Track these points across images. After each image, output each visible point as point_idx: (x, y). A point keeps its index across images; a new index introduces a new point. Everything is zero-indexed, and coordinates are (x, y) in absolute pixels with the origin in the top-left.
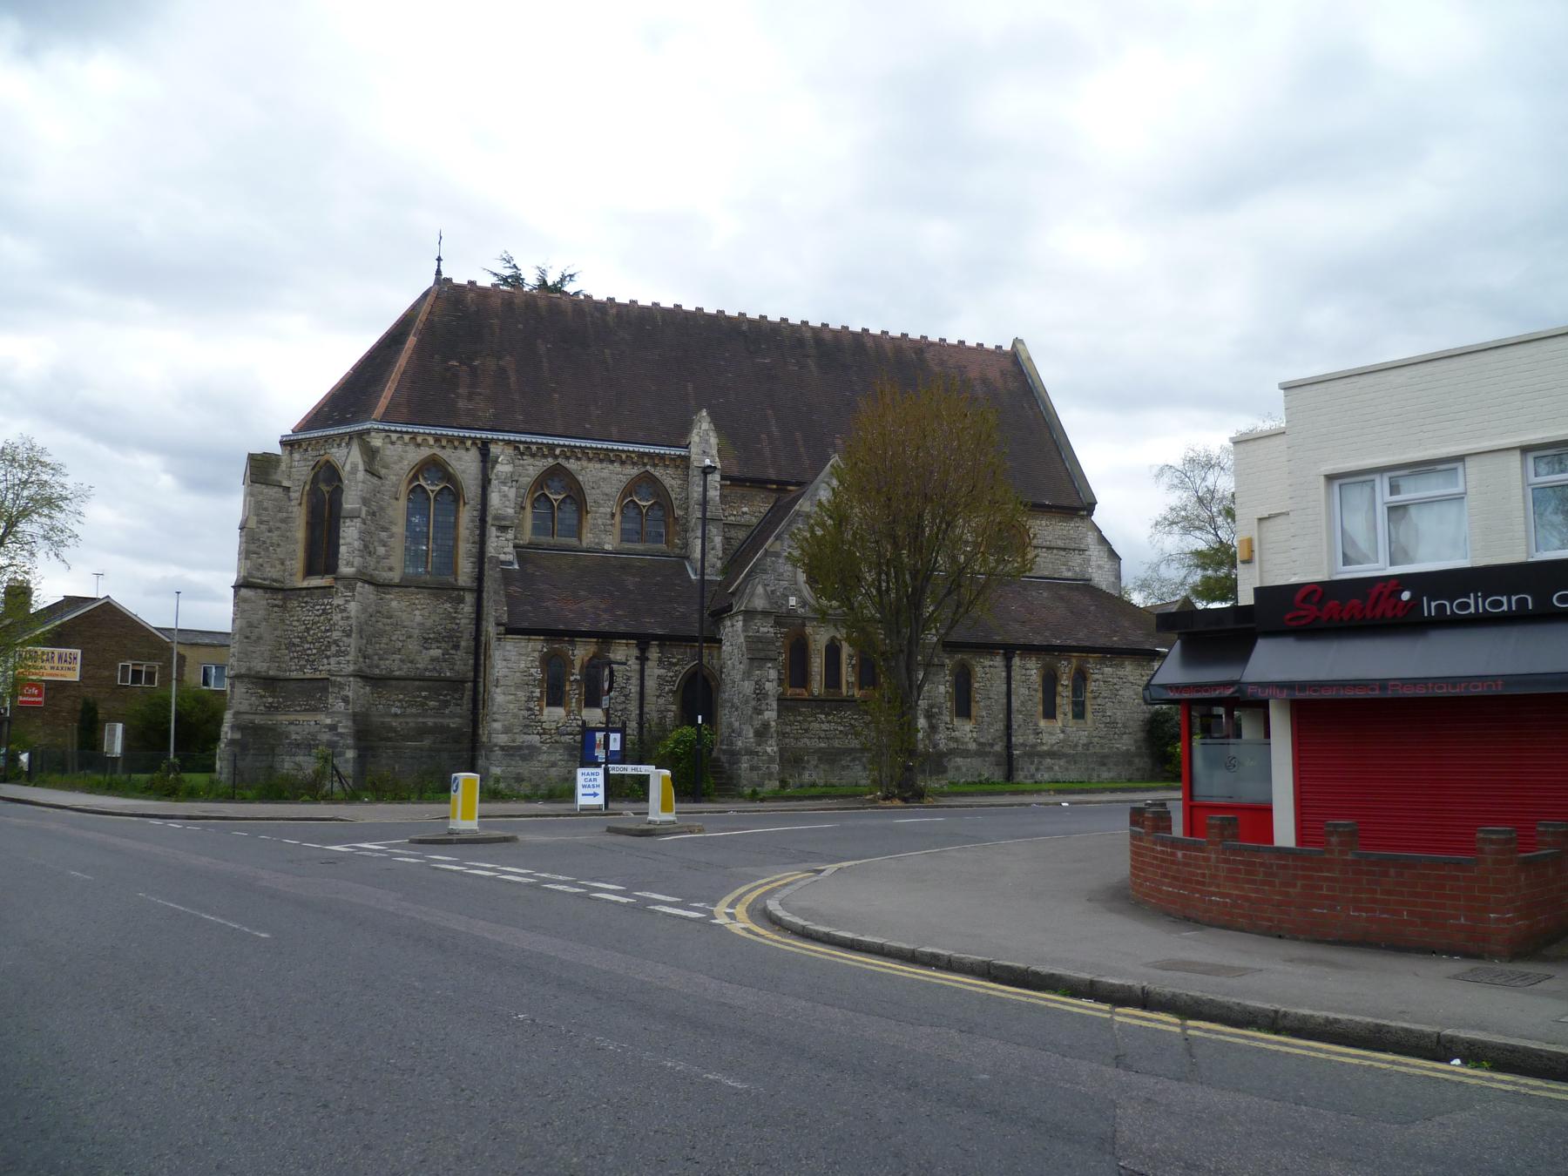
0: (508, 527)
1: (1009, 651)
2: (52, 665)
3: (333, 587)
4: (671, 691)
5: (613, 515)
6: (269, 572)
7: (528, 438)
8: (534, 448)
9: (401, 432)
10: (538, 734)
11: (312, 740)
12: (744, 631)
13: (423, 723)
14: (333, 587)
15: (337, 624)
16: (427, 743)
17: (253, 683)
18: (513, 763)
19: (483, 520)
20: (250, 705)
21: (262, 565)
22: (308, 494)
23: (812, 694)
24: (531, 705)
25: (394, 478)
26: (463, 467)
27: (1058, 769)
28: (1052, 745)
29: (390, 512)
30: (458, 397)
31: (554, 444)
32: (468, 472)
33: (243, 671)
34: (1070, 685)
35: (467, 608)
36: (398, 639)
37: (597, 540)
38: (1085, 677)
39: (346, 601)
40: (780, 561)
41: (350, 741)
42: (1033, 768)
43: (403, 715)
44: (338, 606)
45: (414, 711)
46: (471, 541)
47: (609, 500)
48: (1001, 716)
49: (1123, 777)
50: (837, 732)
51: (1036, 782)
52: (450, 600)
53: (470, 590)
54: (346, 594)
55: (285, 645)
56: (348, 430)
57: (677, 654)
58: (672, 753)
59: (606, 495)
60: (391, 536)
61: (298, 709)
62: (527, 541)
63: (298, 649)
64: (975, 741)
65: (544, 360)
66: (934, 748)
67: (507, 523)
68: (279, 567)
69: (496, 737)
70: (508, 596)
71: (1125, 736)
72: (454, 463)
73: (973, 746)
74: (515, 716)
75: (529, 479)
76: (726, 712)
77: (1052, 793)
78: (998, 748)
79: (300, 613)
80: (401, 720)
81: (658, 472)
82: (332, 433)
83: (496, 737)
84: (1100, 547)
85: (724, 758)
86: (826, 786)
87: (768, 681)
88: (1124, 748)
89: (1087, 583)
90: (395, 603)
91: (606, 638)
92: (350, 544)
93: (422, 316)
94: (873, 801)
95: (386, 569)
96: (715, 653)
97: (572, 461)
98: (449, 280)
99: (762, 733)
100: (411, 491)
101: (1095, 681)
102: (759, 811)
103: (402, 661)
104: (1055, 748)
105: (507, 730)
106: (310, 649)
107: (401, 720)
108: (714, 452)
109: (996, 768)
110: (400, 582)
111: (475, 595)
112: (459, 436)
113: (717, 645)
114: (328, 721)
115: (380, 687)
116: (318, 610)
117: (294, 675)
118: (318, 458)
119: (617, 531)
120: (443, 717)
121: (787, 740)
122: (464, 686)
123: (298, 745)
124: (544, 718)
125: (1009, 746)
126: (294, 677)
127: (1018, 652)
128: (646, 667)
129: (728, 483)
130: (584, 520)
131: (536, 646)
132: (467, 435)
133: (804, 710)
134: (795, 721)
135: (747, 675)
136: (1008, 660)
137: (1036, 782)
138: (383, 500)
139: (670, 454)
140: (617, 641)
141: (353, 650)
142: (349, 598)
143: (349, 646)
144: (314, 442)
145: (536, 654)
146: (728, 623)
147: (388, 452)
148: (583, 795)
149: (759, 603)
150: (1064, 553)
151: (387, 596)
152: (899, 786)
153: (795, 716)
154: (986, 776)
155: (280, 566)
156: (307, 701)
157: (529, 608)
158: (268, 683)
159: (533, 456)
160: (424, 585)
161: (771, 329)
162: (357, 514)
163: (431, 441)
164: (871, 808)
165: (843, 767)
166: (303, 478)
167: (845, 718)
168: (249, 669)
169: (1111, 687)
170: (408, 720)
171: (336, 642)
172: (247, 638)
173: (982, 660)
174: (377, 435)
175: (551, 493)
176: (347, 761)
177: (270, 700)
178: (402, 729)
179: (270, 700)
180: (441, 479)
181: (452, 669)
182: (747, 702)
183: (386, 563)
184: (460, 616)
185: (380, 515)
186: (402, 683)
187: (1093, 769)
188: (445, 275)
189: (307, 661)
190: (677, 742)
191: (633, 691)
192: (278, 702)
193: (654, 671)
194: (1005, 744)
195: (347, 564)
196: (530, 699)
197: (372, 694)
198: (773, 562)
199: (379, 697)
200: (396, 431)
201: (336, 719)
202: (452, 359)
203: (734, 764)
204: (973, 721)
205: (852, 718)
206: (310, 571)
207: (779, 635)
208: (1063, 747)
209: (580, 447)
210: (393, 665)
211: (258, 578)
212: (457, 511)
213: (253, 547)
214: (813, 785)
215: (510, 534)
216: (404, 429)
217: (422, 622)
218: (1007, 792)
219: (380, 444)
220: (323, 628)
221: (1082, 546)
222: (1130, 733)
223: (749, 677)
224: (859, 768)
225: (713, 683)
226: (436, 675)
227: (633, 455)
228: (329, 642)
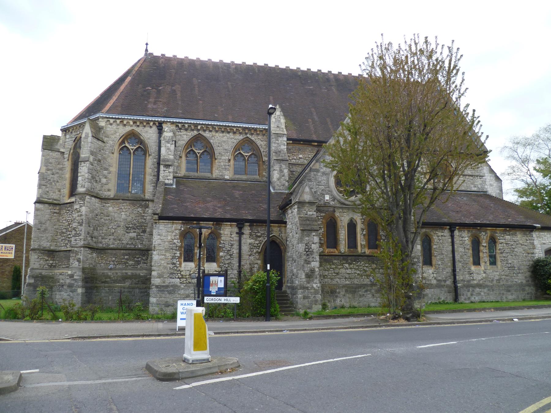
0: (170, 165)
1: (452, 227)
2: (2, 251)
4: (257, 252)
5: (229, 160)
6: (52, 195)
7: (183, 121)
8: (186, 125)
9: (115, 118)
10: (178, 278)
12: (298, 214)
13: (126, 273)
16: (127, 284)
17: (42, 253)
18: (164, 295)
19: (159, 164)
21: (48, 192)
22: (72, 155)
23: (341, 252)
24: (175, 261)
25: (112, 142)
27: (483, 294)
28: (479, 280)
29: (109, 160)
30: (148, 103)
31: (197, 123)
32: (151, 138)
34: (487, 246)
36: (112, 228)
38: (495, 241)
39: (80, 206)
40: (319, 174)
41: (80, 283)
42: (469, 294)
43: (114, 269)
44: (77, 209)
45: (121, 266)
46: (152, 175)
47: (227, 152)
48: (450, 264)
49: (520, 298)
50: (356, 275)
51: (472, 302)
52: (141, 206)
54: (80, 202)
55: (60, 233)
57: (261, 230)
58: (252, 289)
59: (226, 150)
60: (110, 173)
61: (64, 266)
62: (183, 175)
63: (65, 235)
64: (435, 279)
65: (196, 87)
66: (416, 283)
67: (169, 163)
70: (165, 200)
71: (519, 275)
72: (143, 134)
73: (434, 282)
74: (165, 268)
75: (184, 142)
76: (290, 263)
77: (493, 310)
78: (449, 282)
79: (66, 216)
80: (113, 272)
81: (253, 138)
82: (82, 122)
84: (491, 175)
85: (289, 291)
86: (350, 307)
87: (313, 243)
88: (520, 281)
89: (485, 193)
90: (111, 208)
91: (219, 221)
92: (83, 175)
93: (136, 69)
94: (386, 320)
95: (106, 190)
96: (283, 229)
97: (207, 132)
98: (152, 54)
99: (310, 276)
100: (121, 149)
101: (501, 244)
102: (306, 330)
103: (114, 239)
104: (481, 282)
105: (160, 276)
106: (70, 234)
107: (113, 272)
108: (283, 126)
109: (448, 294)
110: (114, 197)
113: (284, 225)
114: (70, 272)
115: (102, 254)
117: (63, 249)
118: (77, 136)
119: (232, 169)
120: (137, 270)
121: (326, 280)
124: (182, 269)
125: (455, 281)
126: (63, 250)
127: (457, 227)
128: (242, 238)
129: (291, 142)
130: (214, 163)
131: (177, 227)
132: (150, 119)
133: (335, 261)
134: (331, 268)
135: (301, 240)
136: (452, 232)
137: (472, 302)
138: (105, 154)
139: (260, 128)
140: (225, 223)
141: (83, 233)
142: (82, 205)
143: (81, 231)
144: (75, 128)
145: (177, 232)
146: (290, 211)
147: (108, 129)
148: (181, 319)
149: (307, 197)
150: (472, 178)
151: (107, 205)
152: (403, 310)
153: (331, 265)
154: (443, 299)
157: (176, 206)
159: (186, 130)
161: (313, 74)
162: (87, 160)
163: (131, 123)
164: (385, 326)
165: (360, 295)
167: (360, 266)
168: (40, 246)
169: (510, 247)
170: (117, 271)
171: (74, 229)
172: (39, 229)
173: (437, 232)
174: (102, 120)
175: (196, 150)
176: (78, 294)
177: (51, 262)
178: (114, 277)
179: (51, 262)
180: (137, 143)
181: (142, 244)
182: (301, 257)
183: (106, 187)
184: (146, 215)
185: (104, 162)
186: (114, 252)
187: (503, 294)
188: (149, 51)
189: (69, 241)
190: (255, 282)
193: (247, 240)
194: (453, 280)
196: (173, 257)
197: (98, 257)
198: (315, 175)
199: (102, 259)
200: (112, 118)
202: (149, 87)
203: (294, 294)
204: (434, 267)
205: (365, 266)
207: (320, 218)
208: (485, 281)
209: (211, 125)
210: (110, 242)
212: (145, 159)
213: (43, 182)
214: (343, 307)
215: (171, 169)
216: (117, 117)
218: (465, 310)
219: (104, 125)
221: (481, 174)
222: (522, 273)
223: (301, 241)
224: (370, 296)
225: (282, 247)
226: (133, 247)
227: (240, 129)
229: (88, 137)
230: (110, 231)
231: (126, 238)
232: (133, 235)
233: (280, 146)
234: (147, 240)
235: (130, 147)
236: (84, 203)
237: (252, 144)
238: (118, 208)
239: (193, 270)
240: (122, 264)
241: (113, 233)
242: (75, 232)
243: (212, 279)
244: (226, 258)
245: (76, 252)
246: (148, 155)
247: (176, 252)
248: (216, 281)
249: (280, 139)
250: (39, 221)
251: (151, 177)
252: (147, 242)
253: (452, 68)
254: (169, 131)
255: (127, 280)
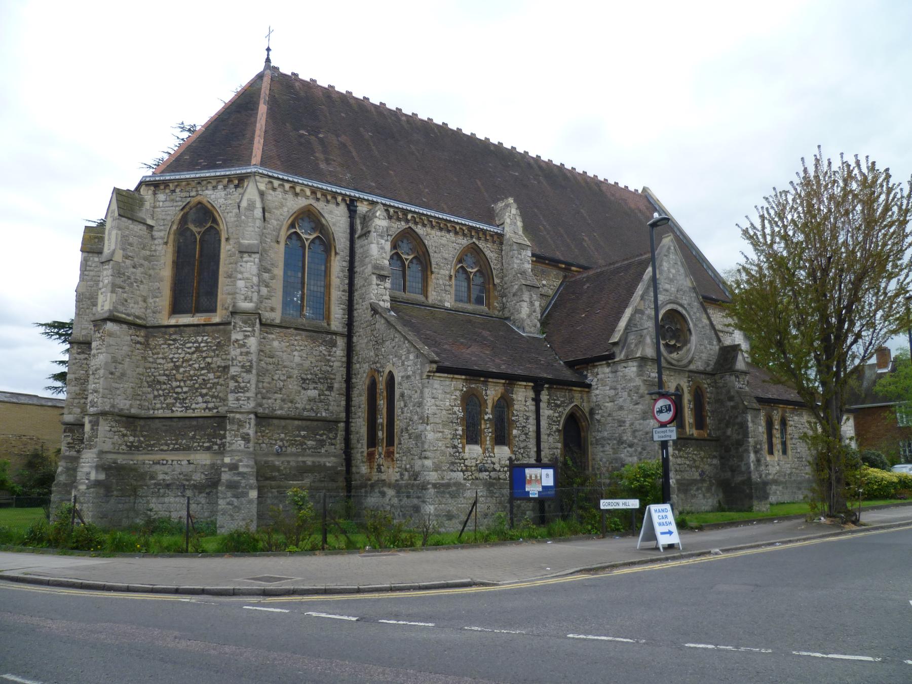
3: (229, 323)
6: (132, 308)
9: (283, 180)
10: (462, 471)
11: (187, 480)
14: (229, 323)
15: (236, 359)
16: (307, 481)
17: (116, 421)
20: (113, 443)
22: (175, 234)
24: (456, 442)
25: (275, 223)
26: (334, 220)
29: (272, 254)
31: (407, 210)
32: (338, 225)
33: (107, 408)
35: (339, 351)
36: (279, 379)
37: (439, 298)
41: (253, 481)
44: (237, 341)
45: (294, 450)
53: (341, 335)
54: (245, 329)
55: (148, 382)
56: (228, 173)
57: (561, 396)
59: (445, 259)
60: (273, 278)
61: (165, 448)
63: (164, 386)
68: (141, 304)
69: (429, 475)
72: (326, 215)
74: (443, 453)
81: (481, 244)
82: (208, 175)
83: (429, 475)
90: (276, 343)
91: (511, 379)
92: (248, 279)
95: (268, 309)
98: (276, 69)
103: (283, 400)
104: (776, 477)
105: (437, 468)
110: (281, 323)
111: (345, 340)
112: (332, 191)
113: (587, 390)
115: (264, 426)
116: (190, 348)
117: (160, 413)
118: (189, 199)
120: (321, 456)
122: (337, 426)
123: (168, 486)
124: (466, 456)
132: (339, 191)
141: (254, 386)
142: (249, 333)
143: (249, 382)
145: (458, 393)
151: (269, 336)
155: (142, 303)
156: (177, 440)
158: (129, 420)
160: (302, 327)
162: (256, 250)
163: (308, 193)
166: (169, 218)
168: (113, 406)
171: (234, 378)
172: (112, 373)
174: (261, 180)
176: (250, 502)
177: (131, 439)
178: (285, 468)
179: (131, 439)
180: (314, 230)
181: (328, 410)
183: (268, 303)
184: (333, 359)
186: (283, 423)
189: (176, 399)
191: (531, 430)
192: (139, 441)
195: (246, 299)
196: (455, 436)
199: (263, 436)
200: (278, 179)
201: (237, 458)
206: (176, 308)
209: (426, 215)
210: (276, 405)
211: (122, 313)
213: (119, 281)
216: (286, 178)
217: (301, 362)
220: (196, 366)
224: (701, 496)
225: (583, 424)
226: (314, 415)
228: (204, 379)
229: (255, 207)
230: (276, 384)
231: (302, 399)
232: (313, 393)
233: (523, 264)
234: (335, 404)
235: (304, 236)
236: (254, 330)
237: (478, 254)
238: (288, 344)
239: (480, 458)
240: (297, 445)
241: (281, 389)
242: (237, 384)
243: (528, 471)
244: (521, 439)
245: (240, 421)
246: (333, 253)
247: (457, 427)
248: (538, 475)
249: (524, 253)
250: (113, 357)
251: (340, 293)
252: (336, 408)
253: (890, 201)
254: (381, 217)
255: (306, 475)
